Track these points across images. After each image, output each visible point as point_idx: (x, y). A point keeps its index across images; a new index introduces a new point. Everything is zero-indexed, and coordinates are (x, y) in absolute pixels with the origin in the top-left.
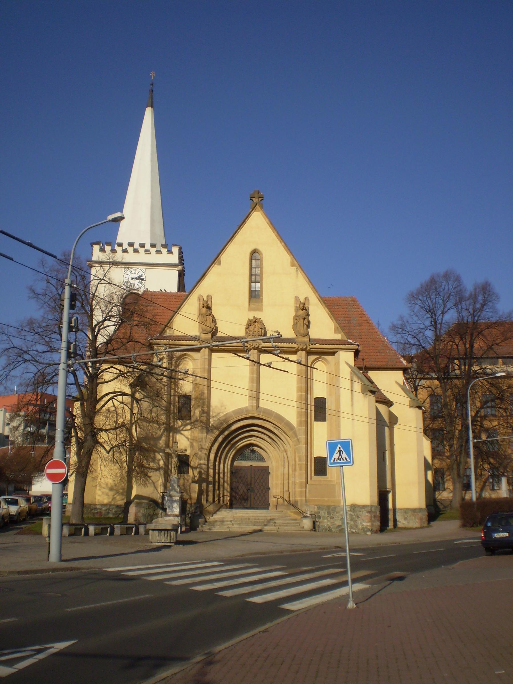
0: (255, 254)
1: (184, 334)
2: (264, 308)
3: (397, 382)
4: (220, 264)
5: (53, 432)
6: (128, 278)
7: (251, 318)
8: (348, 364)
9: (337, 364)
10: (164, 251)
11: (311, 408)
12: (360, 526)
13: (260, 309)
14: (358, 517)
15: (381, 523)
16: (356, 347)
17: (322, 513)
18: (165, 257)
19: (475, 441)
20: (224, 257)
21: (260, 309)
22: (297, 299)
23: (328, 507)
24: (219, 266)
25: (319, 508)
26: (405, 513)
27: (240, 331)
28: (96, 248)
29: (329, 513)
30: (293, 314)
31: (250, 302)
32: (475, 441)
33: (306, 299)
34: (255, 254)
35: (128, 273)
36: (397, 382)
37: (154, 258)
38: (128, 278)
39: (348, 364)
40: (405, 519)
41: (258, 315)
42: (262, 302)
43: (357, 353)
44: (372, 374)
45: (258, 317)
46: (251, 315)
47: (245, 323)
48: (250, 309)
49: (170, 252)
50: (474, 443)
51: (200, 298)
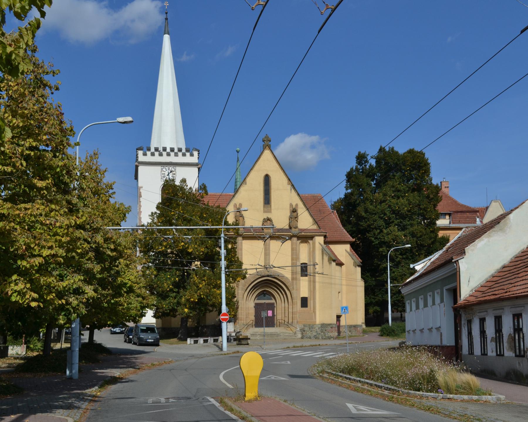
0: (267, 179)
1: (264, 250)
2: (272, 210)
3: (346, 251)
4: (246, 184)
5: (403, 323)
6: (164, 174)
7: (266, 218)
8: (320, 244)
9: (314, 244)
10: (188, 154)
11: (299, 269)
12: (327, 335)
13: (270, 212)
14: (326, 330)
15: (338, 333)
16: (325, 234)
17: (306, 329)
18: (188, 159)
19: (391, 285)
20: (248, 180)
21: (270, 212)
22: (291, 205)
23: (309, 325)
24: (245, 186)
25: (304, 326)
26: (350, 328)
27: (258, 224)
28: (140, 153)
29: (310, 328)
30: (289, 214)
31: (264, 207)
32: (391, 285)
33: (297, 205)
34: (267, 179)
35: (164, 170)
36: (346, 251)
37: (180, 159)
38: (164, 174)
39: (320, 244)
40: (350, 331)
41: (269, 216)
42: (271, 207)
43: (325, 237)
44: (332, 247)
45: (270, 217)
46: (265, 216)
47: (262, 220)
48: (264, 212)
49: (192, 155)
50: (391, 286)
51: (235, 205)
